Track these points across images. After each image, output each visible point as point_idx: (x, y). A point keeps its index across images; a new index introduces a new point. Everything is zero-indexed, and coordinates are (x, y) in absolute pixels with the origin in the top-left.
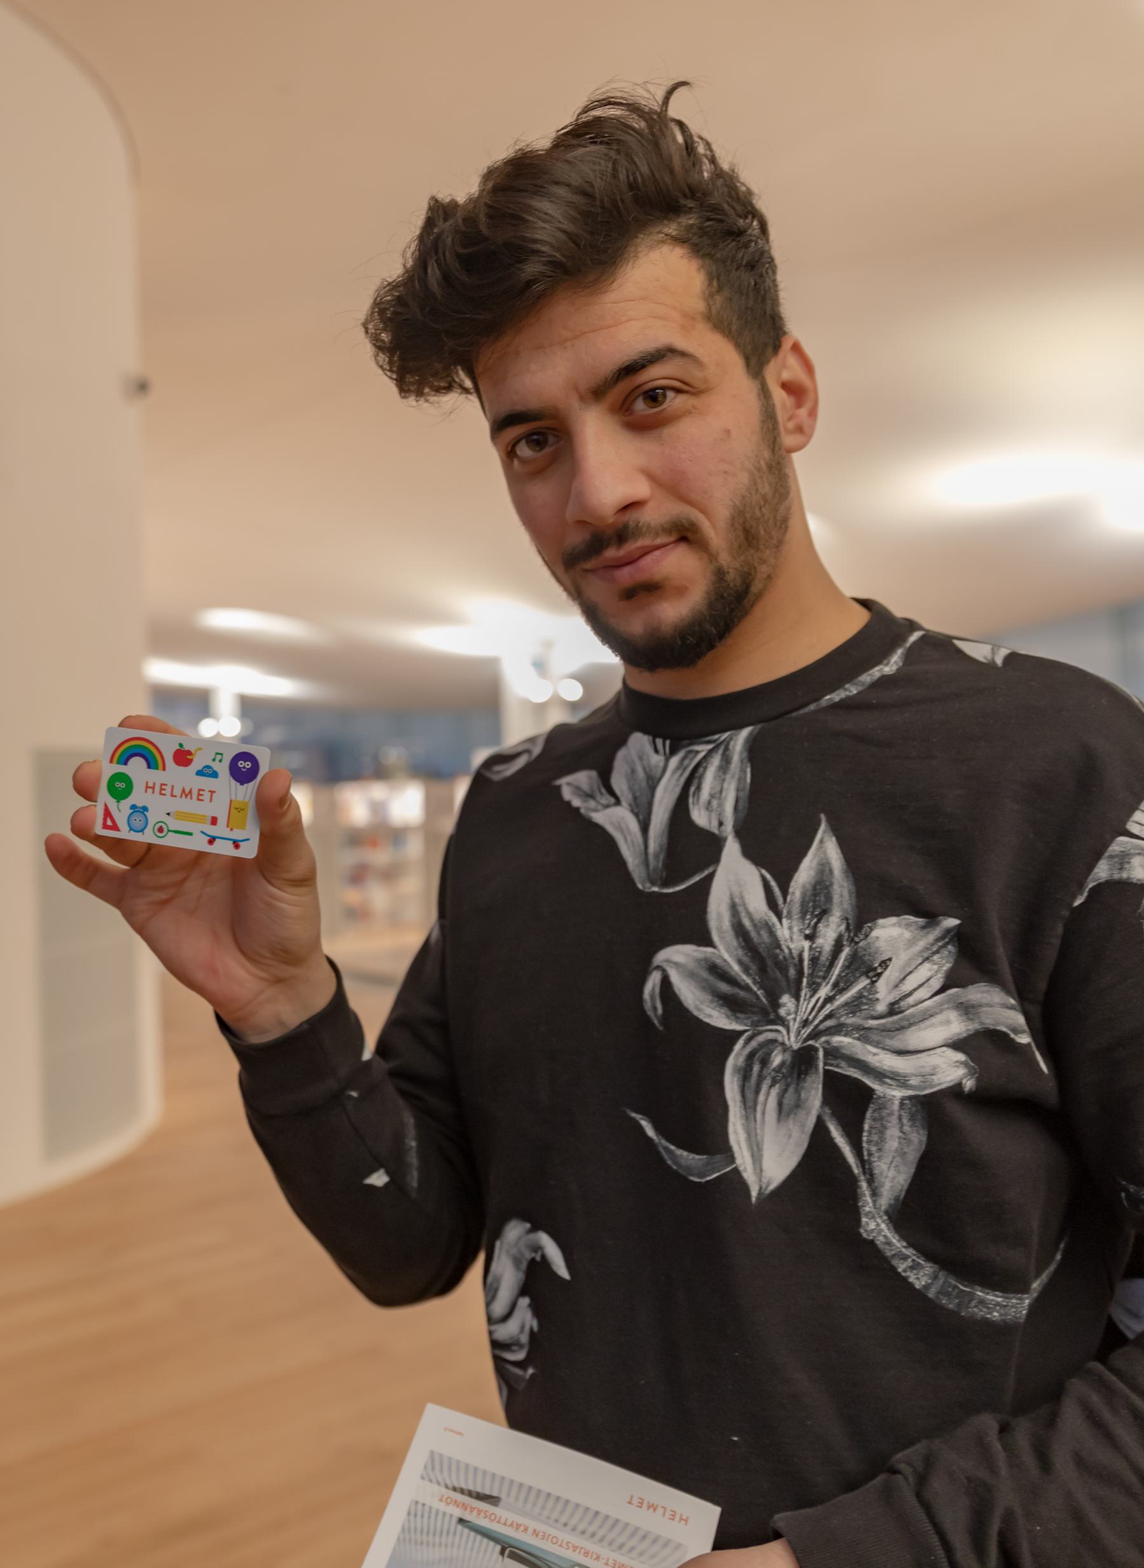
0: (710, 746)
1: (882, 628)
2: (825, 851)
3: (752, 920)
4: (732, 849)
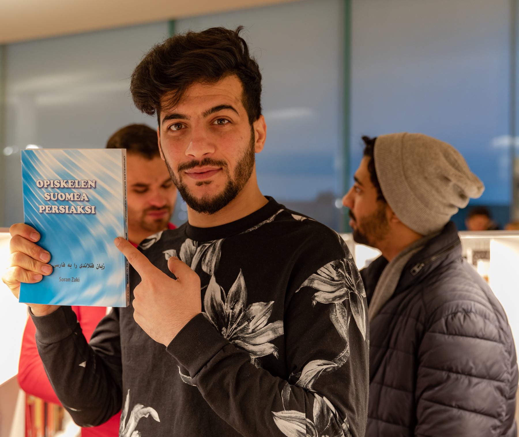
0: (210, 244)
1: (271, 205)
2: (240, 281)
3: (216, 303)
4: (213, 279)
